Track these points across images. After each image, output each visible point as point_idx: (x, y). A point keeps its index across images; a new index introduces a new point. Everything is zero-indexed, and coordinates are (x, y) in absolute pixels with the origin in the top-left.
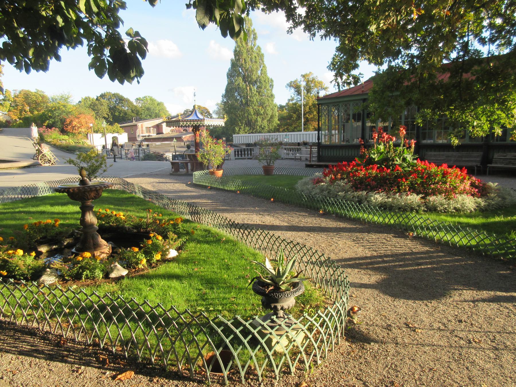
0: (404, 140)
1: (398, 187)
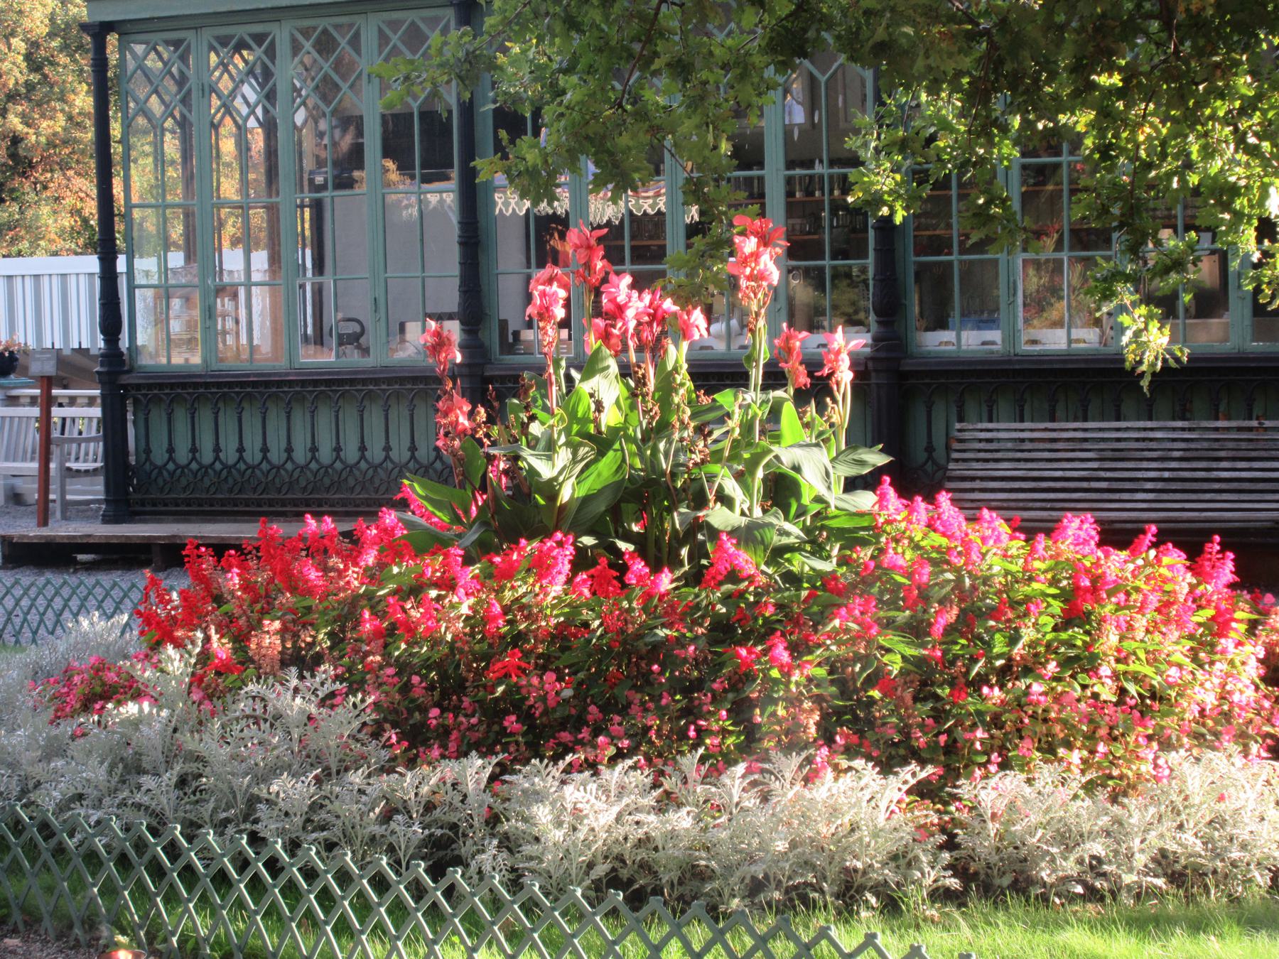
0: (773, 332)
1: (741, 710)
